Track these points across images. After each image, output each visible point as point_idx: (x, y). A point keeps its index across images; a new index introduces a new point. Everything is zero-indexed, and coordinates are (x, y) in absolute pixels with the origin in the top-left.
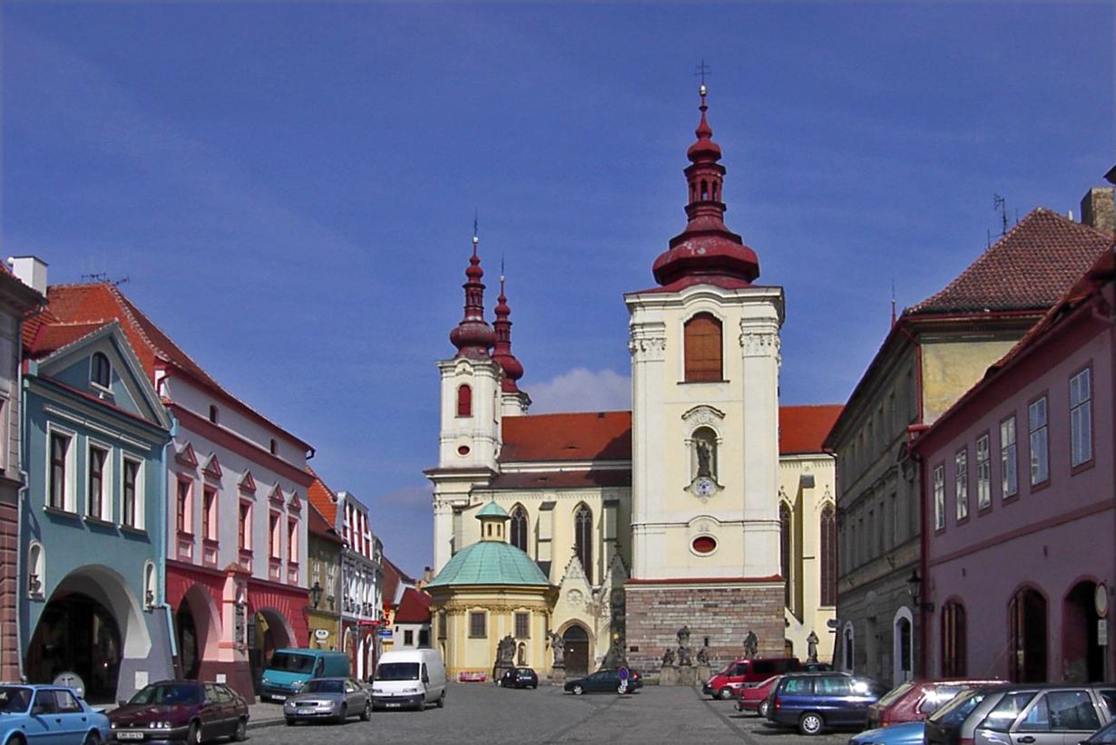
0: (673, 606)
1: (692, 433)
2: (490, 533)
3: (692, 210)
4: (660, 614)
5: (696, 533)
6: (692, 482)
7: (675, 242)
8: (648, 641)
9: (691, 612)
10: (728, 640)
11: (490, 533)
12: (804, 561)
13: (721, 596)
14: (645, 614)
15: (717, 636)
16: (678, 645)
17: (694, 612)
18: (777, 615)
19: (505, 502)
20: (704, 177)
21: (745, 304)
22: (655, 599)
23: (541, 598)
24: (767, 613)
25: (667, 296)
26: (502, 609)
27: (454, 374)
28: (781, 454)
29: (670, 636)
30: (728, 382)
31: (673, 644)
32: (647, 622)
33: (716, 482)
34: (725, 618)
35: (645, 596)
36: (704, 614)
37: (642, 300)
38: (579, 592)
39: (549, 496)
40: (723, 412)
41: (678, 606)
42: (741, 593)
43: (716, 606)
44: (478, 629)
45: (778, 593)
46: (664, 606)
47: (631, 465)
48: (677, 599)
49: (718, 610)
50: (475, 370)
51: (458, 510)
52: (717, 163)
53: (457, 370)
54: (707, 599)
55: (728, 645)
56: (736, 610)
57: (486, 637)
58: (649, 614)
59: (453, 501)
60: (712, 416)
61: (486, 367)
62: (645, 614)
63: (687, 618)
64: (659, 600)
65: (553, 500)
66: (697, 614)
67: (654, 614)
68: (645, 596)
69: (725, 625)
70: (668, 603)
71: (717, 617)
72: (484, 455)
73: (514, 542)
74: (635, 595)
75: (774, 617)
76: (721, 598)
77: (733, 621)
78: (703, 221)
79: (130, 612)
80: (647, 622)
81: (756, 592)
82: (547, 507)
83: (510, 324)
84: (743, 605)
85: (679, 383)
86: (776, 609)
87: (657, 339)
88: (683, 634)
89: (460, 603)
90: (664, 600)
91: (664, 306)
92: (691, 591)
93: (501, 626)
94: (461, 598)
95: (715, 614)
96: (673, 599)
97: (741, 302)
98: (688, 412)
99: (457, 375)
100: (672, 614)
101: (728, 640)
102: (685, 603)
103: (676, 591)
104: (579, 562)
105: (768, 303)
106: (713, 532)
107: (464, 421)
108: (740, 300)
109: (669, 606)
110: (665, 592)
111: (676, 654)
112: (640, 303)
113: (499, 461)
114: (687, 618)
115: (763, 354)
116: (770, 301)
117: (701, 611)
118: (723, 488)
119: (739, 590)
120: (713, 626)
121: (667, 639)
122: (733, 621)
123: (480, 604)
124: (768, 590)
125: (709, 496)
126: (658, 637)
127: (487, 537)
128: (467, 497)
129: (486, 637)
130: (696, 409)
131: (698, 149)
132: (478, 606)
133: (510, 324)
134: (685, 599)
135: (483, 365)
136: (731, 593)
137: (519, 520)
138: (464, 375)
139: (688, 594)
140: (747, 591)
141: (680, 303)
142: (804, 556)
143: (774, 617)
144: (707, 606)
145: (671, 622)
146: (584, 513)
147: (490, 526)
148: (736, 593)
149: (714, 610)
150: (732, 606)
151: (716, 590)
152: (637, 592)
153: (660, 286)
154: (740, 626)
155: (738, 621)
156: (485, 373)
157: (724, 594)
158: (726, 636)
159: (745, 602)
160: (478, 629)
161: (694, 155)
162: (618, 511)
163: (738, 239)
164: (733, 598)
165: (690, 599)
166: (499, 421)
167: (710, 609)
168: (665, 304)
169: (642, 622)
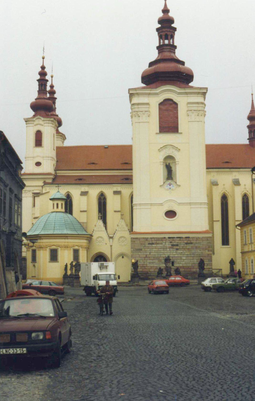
0: (155, 245)
1: (163, 158)
2: (57, 207)
3: (160, 48)
4: (149, 250)
5: (166, 208)
6: (164, 183)
7: (151, 64)
8: (143, 263)
9: (164, 248)
10: (184, 263)
11: (57, 207)
12: (215, 223)
13: (180, 240)
14: (141, 250)
15: (178, 261)
16: (164, 265)
17: (166, 248)
18: (208, 250)
19: (61, 191)
20: (166, 32)
21: (189, 95)
22: (146, 242)
23: (85, 241)
24: (204, 249)
25: (151, 90)
26: (66, 247)
27: (32, 125)
28: (207, 168)
29: (154, 261)
30: (181, 133)
31: (163, 266)
32: (142, 254)
33: (176, 183)
34: (182, 251)
35: (141, 240)
36: (171, 249)
37: (138, 92)
38: (101, 237)
39: (84, 188)
40: (179, 148)
41: (158, 245)
42: (190, 239)
43: (177, 245)
44: (54, 256)
45: (208, 239)
46: (151, 245)
47: (132, 173)
48: (158, 242)
49: (178, 247)
50: (44, 123)
51: (36, 195)
52: (173, 25)
53: (35, 123)
54: (173, 242)
55: (184, 265)
56: (187, 247)
57: (58, 262)
58: (143, 250)
59: (33, 190)
60: (174, 150)
61: (50, 122)
62: (141, 250)
63: (163, 251)
64: (148, 242)
65: (87, 190)
66: (168, 250)
67: (146, 250)
68: (141, 240)
69: (182, 255)
70: (153, 244)
71: (178, 251)
72: (48, 167)
73: (66, 212)
74: (136, 240)
75: (207, 251)
76: (180, 242)
77: (186, 253)
78: (167, 54)
79: (241, 295)
80: (142, 254)
81: (198, 239)
82: (84, 194)
83: (56, 98)
84: (191, 245)
85: (157, 133)
86: (208, 247)
87: (145, 111)
88: (167, 260)
89: (44, 244)
90: (151, 242)
91: (149, 95)
92: (165, 238)
93: (66, 257)
94: (44, 242)
95: (177, 249)
96: (155, 242)
97: (187, 94)
98: (161, 148)
99: (35, 125)
100: (155, 250)
101: (184, 263)
102: (162, 244)
103: (157, 238)
104: (81, 221)
105: (200, 95)
106: (175, 208)
107: (38, 149)
108: (186, 93)
109: (153, 245)
110: (151, 238)
111: (164, 270)
112: (137, 93)
113: (56, 170)
114: (163, 251)
115: (198, 120)
116: (202, 94)
117: (170, 248)
118: (180, 186)
119: (189, 237)
120: (177, 256)
121: (153, 262)
122: (186, 253)
123: (55, 244)
124: (203, 237)
125: (172, 190)
126: (148, 261)
127: (55, 209)
128: (41, 188)
129: (58, 262)
130: (165, 147)
131: (164, 18)
132: (54, 245)
133: (56, 98)
134: (162, 242)
135: (49, 121)
136: (185, 239)
137: (68, 201)
138: (39, 126)
139: (163, 240)
140: (193, 238)
141: (157, 94)
142: (214, 220)
143: (207, 251)
144: (173, 245)
145: (155, 254)
146: (102, 198)
147: (57, 204)
148: (187, 239)
149: (177, 247)
150: (185, 245)
151: (177, 238)
152: (137, 238)
153: (144, 85)
154: (190, 255)
155: (188, 253)
156: (50, 125)
157: (182, 239)
158: (183, 260)
159: (191, 243)
160: (54, 256)
161: (160, 21)
162: (121, 197)
163: (183, 63)
164: (186, 242)
165: (164, 242)
166: (55, 149)
167: (174, 247)
168: (149, 94)
169: (140, 254)
